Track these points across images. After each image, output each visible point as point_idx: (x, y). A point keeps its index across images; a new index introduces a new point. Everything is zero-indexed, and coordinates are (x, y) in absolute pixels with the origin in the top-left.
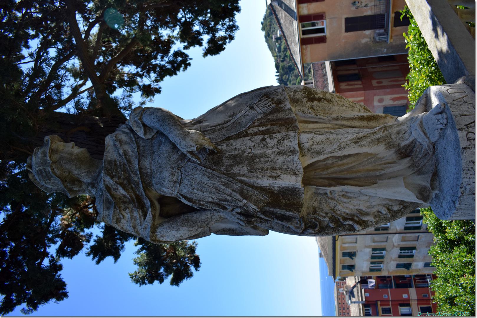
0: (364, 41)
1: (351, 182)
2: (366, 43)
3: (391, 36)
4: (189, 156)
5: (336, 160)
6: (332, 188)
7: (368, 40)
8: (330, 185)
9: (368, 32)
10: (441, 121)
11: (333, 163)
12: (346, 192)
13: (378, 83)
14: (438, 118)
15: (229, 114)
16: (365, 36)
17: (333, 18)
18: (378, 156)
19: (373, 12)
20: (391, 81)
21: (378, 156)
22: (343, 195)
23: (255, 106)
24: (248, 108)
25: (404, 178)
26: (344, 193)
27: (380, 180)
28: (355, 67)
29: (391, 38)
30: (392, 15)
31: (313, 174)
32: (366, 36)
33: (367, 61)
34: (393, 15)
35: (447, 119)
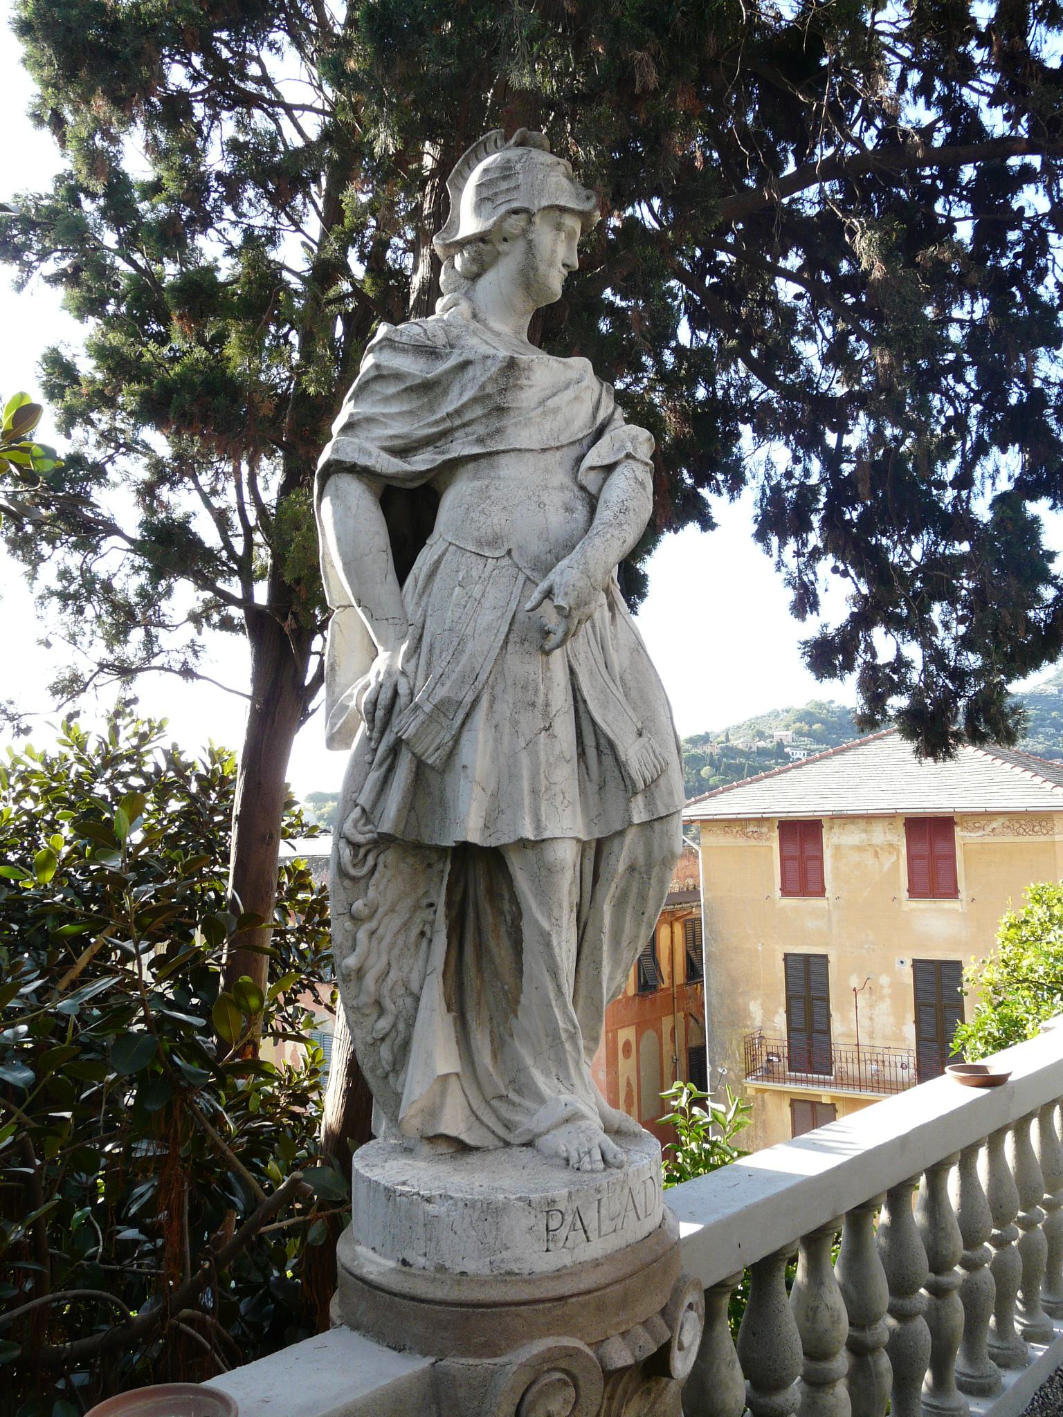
0: (756, 1009)
1: (454, 953)
2: (748, 1015)
3: (764, 1091)
4: (544, 585)
5: (509, 918)
6: (441, 909)
7: (758, 1023)
8: (449, 904)
9: (781, 1020)
10: (586, 1159)
11: (502, 913)
12: (430, 941)
13: (627, 1044)
14: (593, 1152)
15: (628, 677)
16: (768, 1014)
17: (830, 920)
18: (512, 1016)
19: (840, 1041)
20: (629, 1084)
21: (512, 1016)
22: (422, 934)
23: (644, 740)
24: (639, 725)
25: (457, 1074)
26: (428, 934)
27: (455, 1018)
28: (680, 978)
29: (758, 1090)
30: (825, 1094)
31: (480, 869)
32: (769, 1017)
33: (695, 1017)
34: (825, 1100)
35: (592, 1171)
